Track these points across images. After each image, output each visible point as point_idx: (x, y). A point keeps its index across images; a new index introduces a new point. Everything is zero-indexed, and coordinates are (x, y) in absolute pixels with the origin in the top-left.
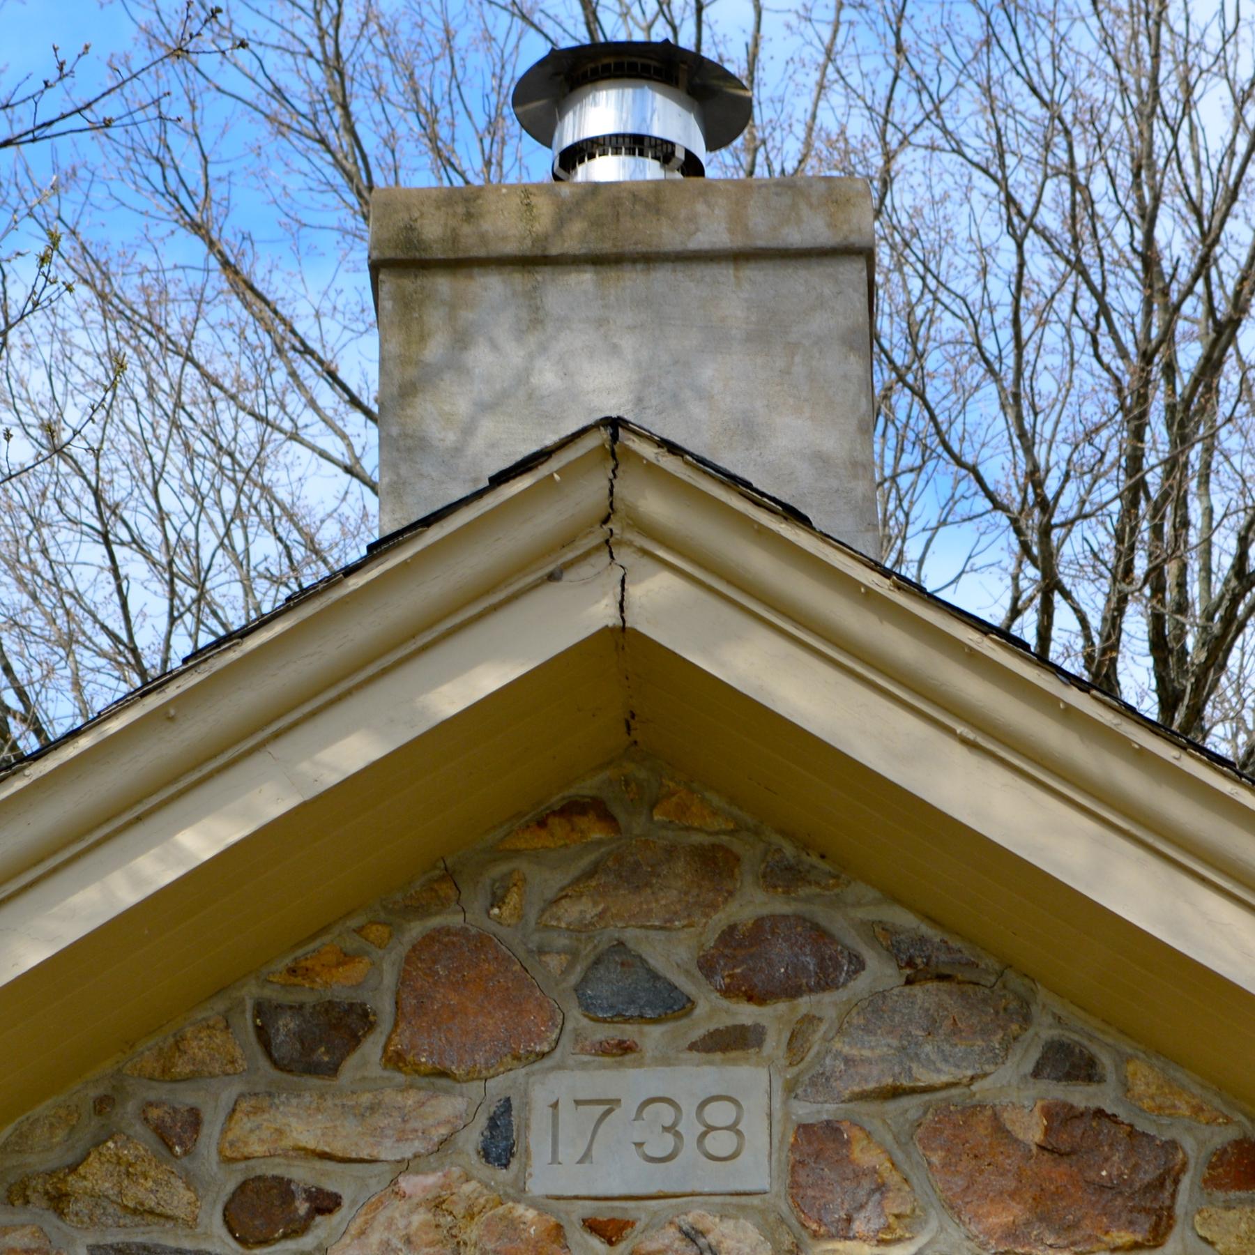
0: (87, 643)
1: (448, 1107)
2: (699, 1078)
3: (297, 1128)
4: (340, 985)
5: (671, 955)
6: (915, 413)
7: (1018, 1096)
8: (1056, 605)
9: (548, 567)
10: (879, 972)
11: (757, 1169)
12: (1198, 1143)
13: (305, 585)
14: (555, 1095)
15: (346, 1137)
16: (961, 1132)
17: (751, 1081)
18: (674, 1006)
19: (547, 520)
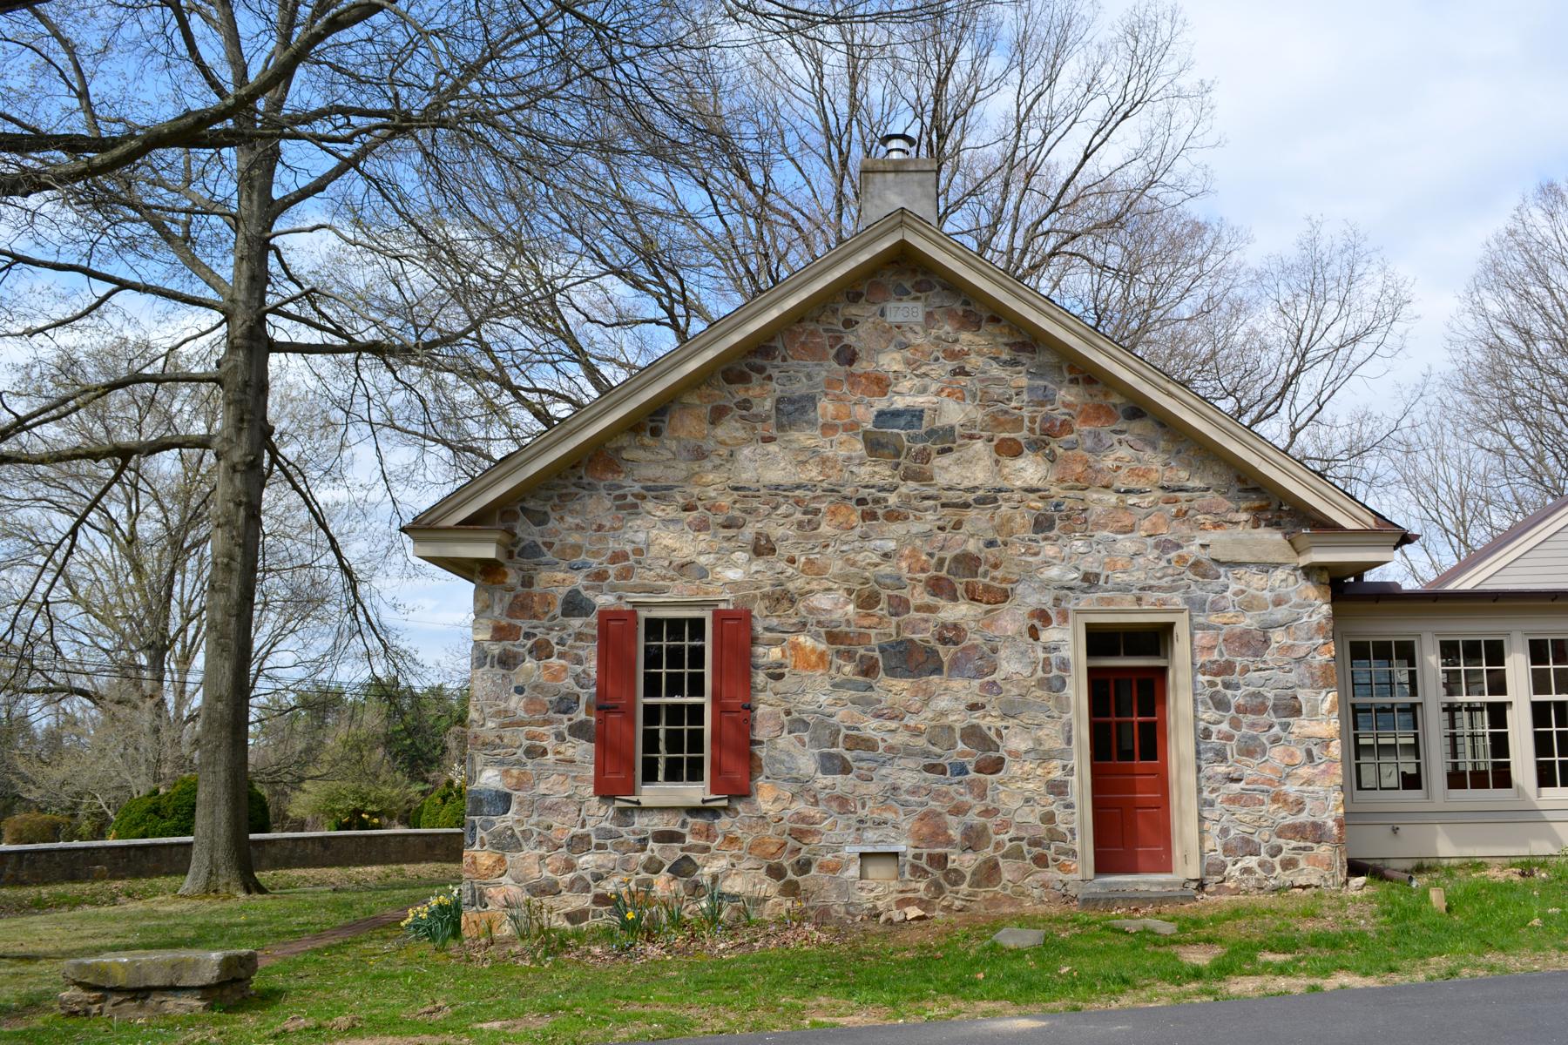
0: (54, 412)
1: (875, 308)
2: (911, 304)
3: (853, 311)
4: (859, 289)
5: (908, 285)
6: (564, 382)
7: (959, 308)
8: (1378, 580)
9: (892, 230)
10: (938, 288)
11: (920, 318)
12: (985, 315)
13: (275, 359)
14: (891, 306)
15: (859, 312)
16: (950, 314)
17: (919, 305)
18: (908, 293)
19: (892, 223)
